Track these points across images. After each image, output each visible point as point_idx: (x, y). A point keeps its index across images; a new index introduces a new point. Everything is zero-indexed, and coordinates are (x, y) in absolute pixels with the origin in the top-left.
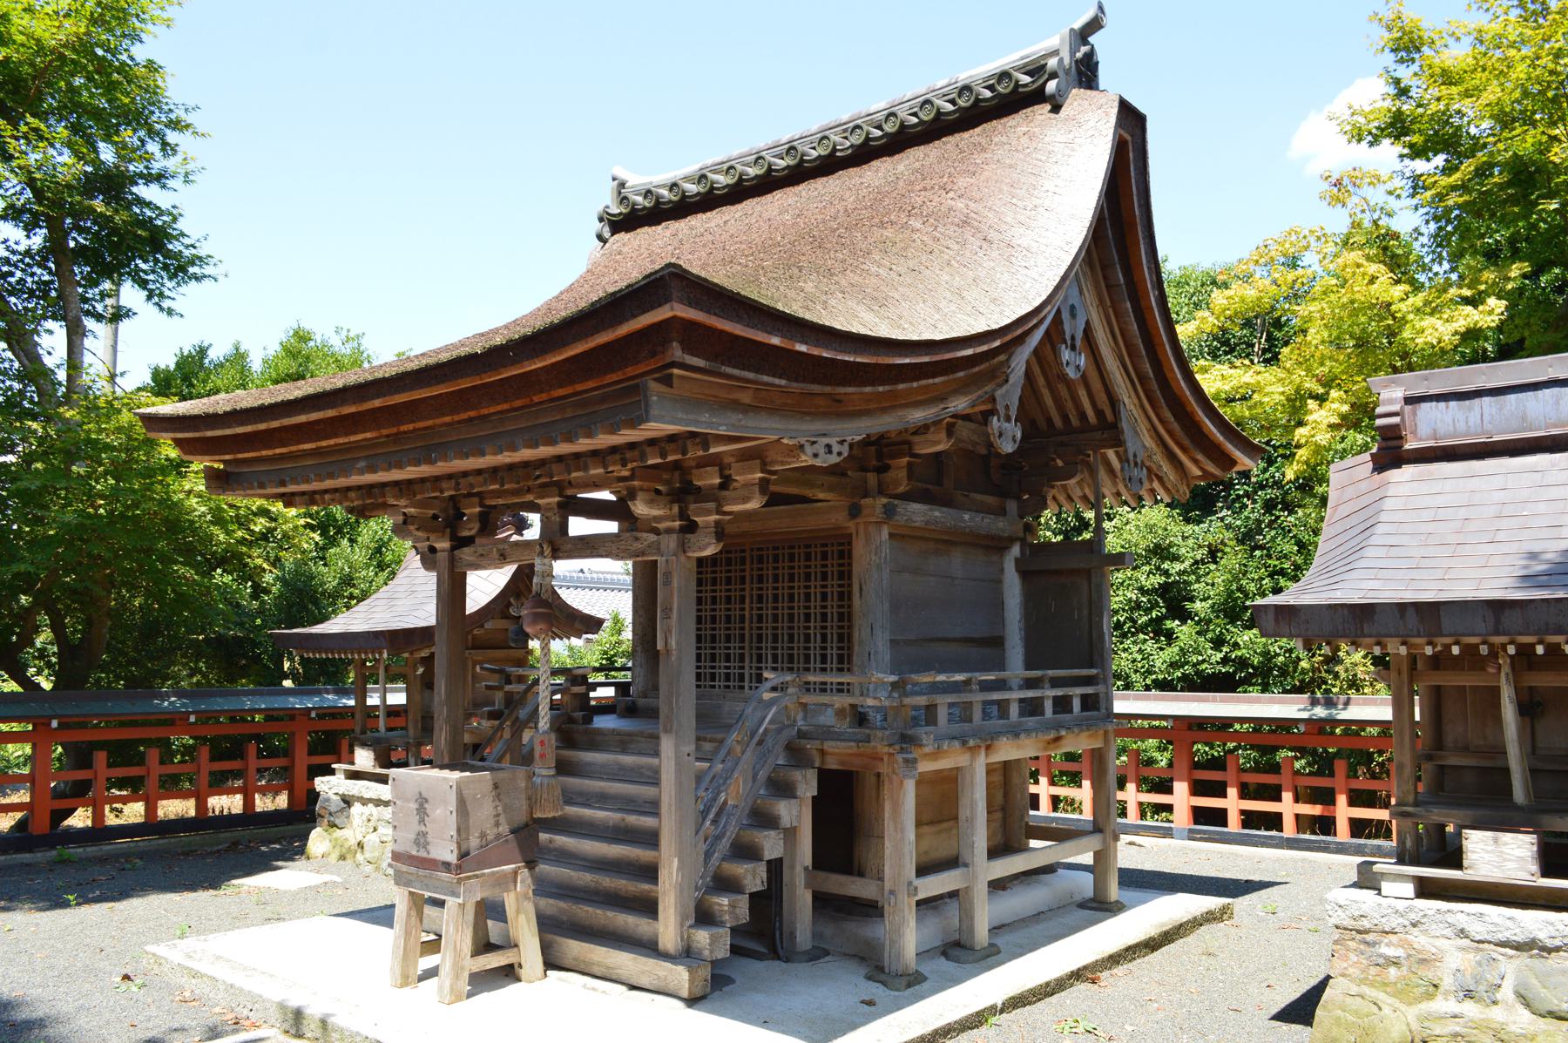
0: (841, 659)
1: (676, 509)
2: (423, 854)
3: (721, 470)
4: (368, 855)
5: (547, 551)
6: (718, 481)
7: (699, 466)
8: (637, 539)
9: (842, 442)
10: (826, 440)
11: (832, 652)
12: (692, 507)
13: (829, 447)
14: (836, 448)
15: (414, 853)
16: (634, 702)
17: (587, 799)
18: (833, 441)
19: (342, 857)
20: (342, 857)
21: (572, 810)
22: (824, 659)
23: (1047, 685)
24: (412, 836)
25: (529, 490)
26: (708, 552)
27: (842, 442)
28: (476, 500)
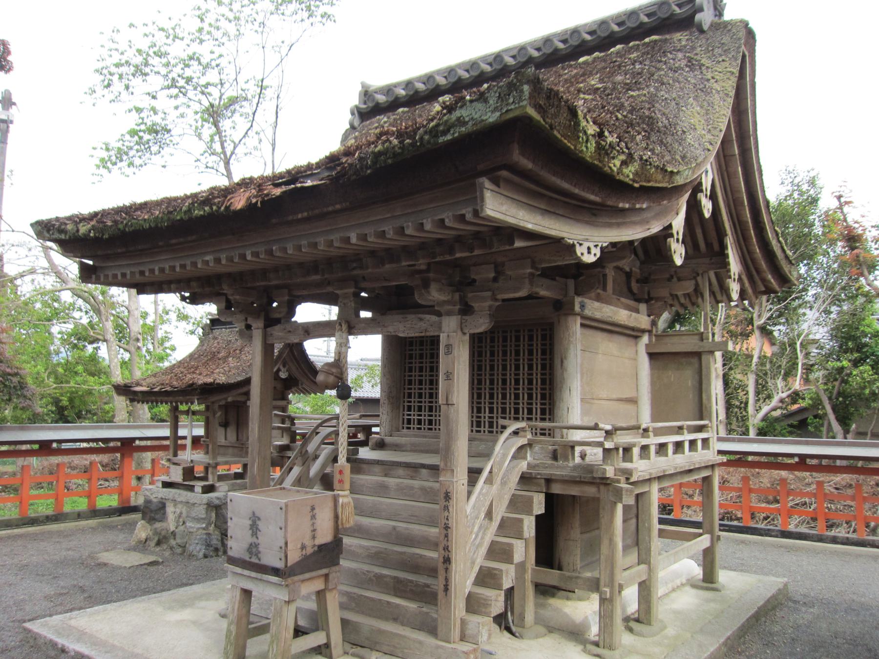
0: (543, 412)
1: (457, 296)
2: (254, 560)
3: (496, 267)
4: (179, 541)
5: (344, 327)
6: (492, 275)
7: (475, 265)
8: (421, 319)
9: (596, 246)
10: (586, 245)
11: (537, 407)
12: (470, 295)
13: (589, 248)
14: (593, 250)
15: (247, 559)
16: (383, 440)
17: (373, 513)
18: (591, 245)
19: (159, 543)
20: (159, 543)
21: (366, 521)
22: (530, 411)
23: (685, 431)
24: (246, 546)
25: (329, 284)
26: (481, 330)
27: (596, 246)
28: (286, 291)
